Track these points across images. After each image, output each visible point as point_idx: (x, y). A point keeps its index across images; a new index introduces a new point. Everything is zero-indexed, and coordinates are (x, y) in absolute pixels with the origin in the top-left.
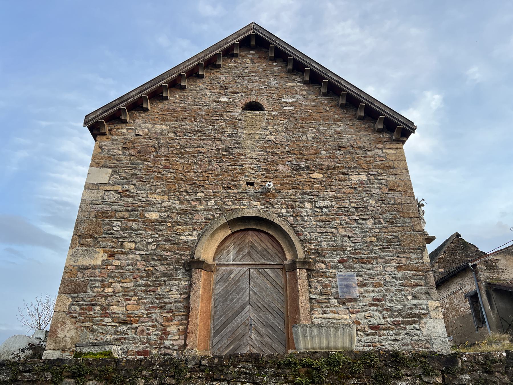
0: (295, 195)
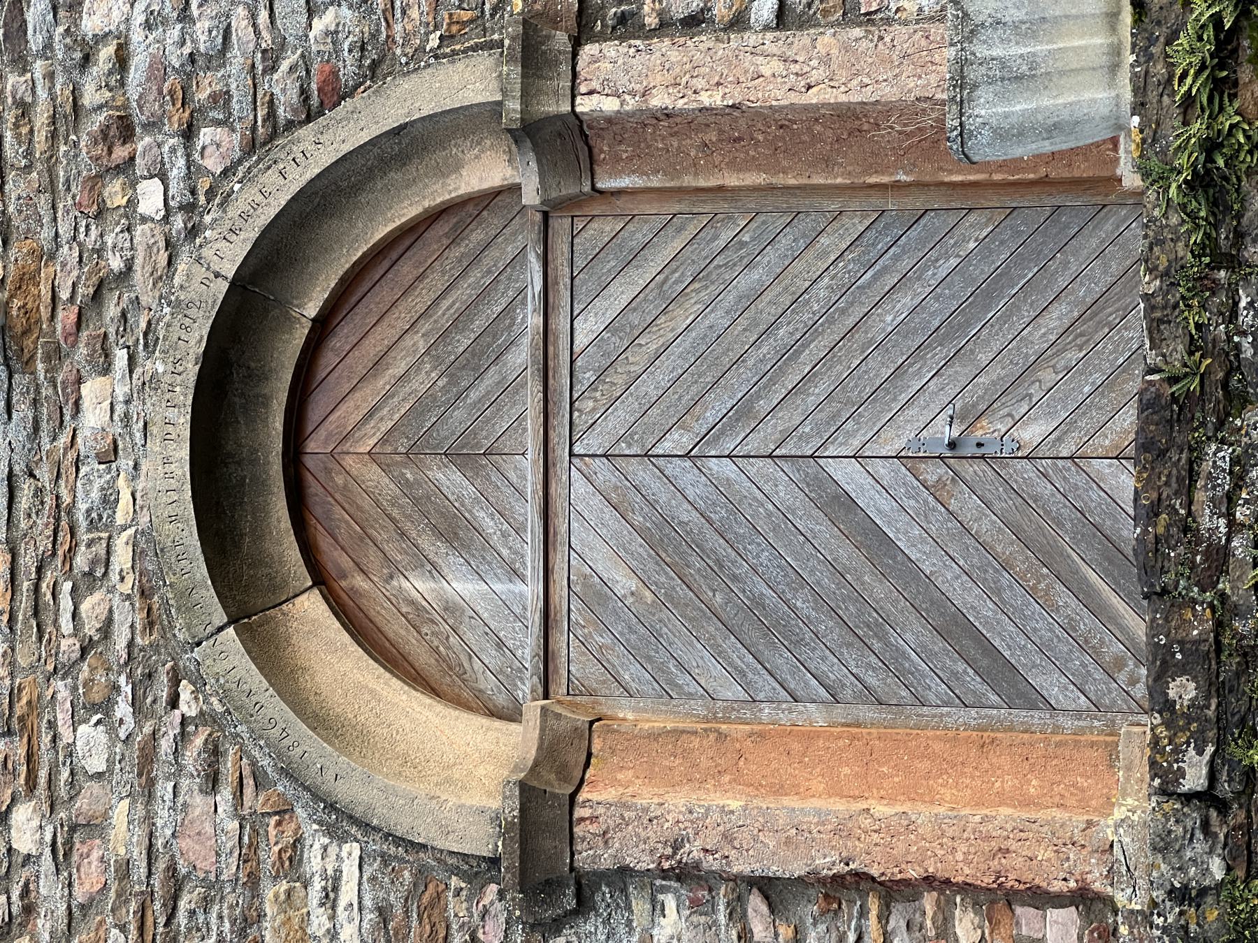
0: (25, 109)
